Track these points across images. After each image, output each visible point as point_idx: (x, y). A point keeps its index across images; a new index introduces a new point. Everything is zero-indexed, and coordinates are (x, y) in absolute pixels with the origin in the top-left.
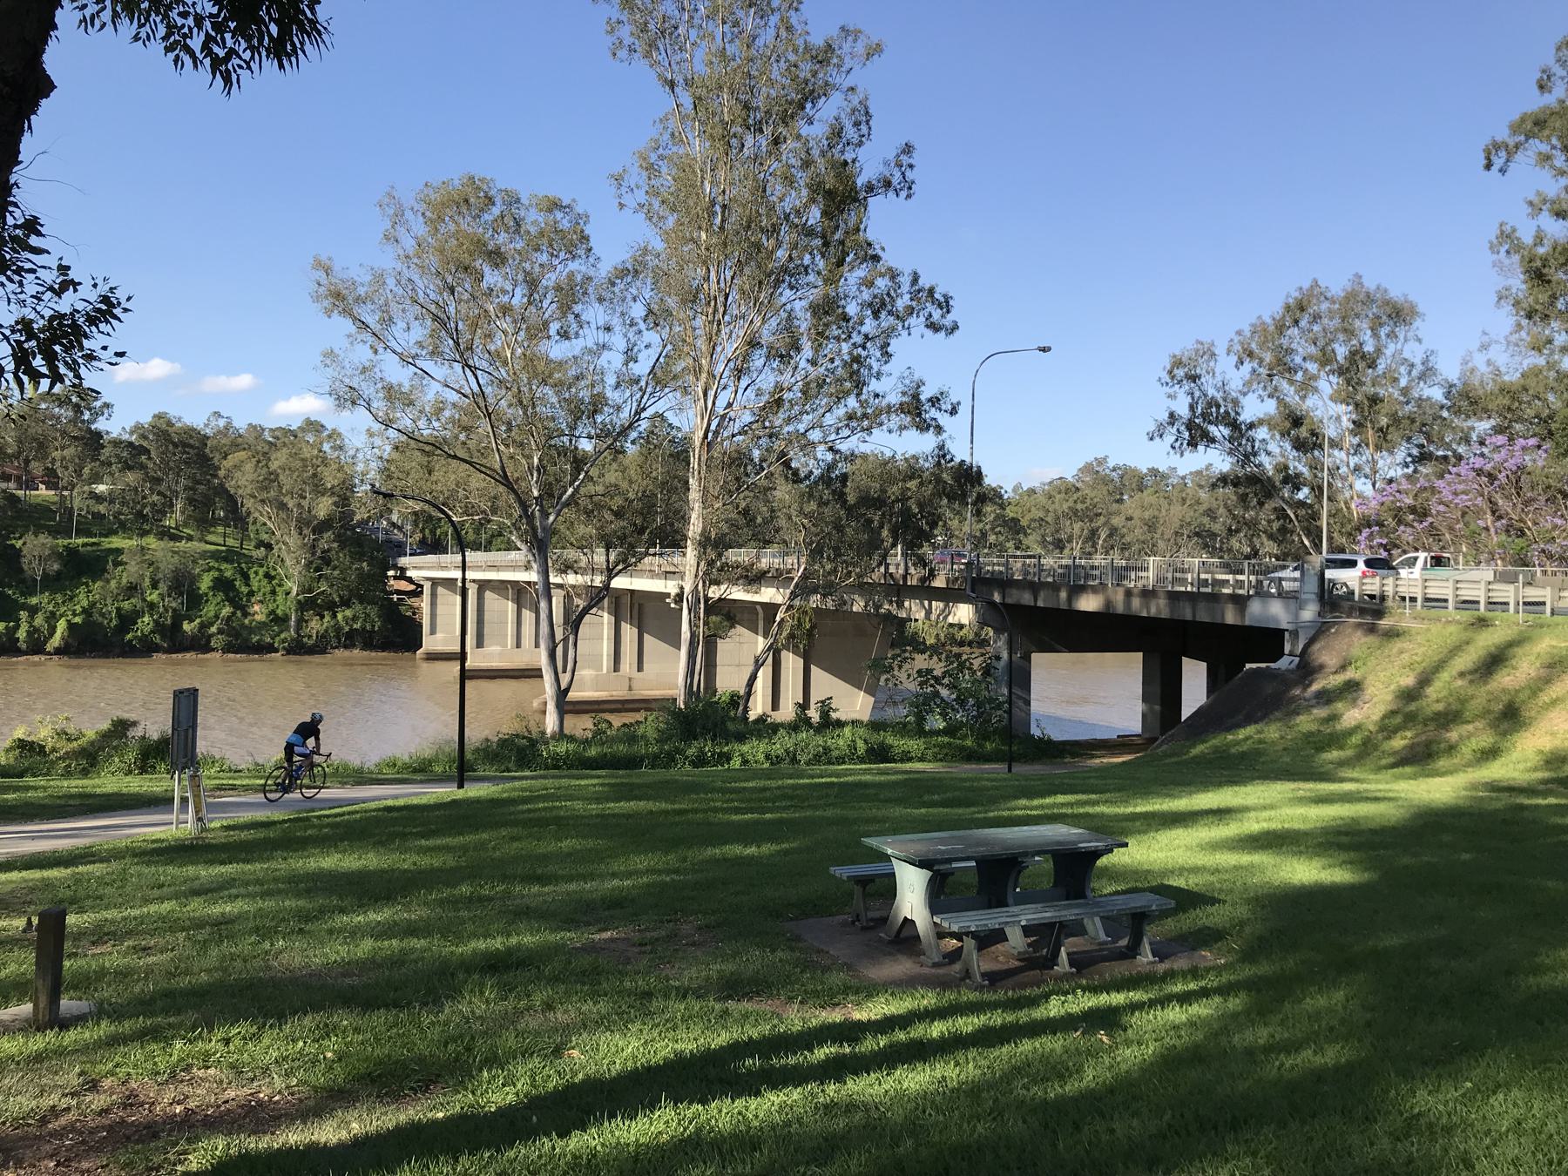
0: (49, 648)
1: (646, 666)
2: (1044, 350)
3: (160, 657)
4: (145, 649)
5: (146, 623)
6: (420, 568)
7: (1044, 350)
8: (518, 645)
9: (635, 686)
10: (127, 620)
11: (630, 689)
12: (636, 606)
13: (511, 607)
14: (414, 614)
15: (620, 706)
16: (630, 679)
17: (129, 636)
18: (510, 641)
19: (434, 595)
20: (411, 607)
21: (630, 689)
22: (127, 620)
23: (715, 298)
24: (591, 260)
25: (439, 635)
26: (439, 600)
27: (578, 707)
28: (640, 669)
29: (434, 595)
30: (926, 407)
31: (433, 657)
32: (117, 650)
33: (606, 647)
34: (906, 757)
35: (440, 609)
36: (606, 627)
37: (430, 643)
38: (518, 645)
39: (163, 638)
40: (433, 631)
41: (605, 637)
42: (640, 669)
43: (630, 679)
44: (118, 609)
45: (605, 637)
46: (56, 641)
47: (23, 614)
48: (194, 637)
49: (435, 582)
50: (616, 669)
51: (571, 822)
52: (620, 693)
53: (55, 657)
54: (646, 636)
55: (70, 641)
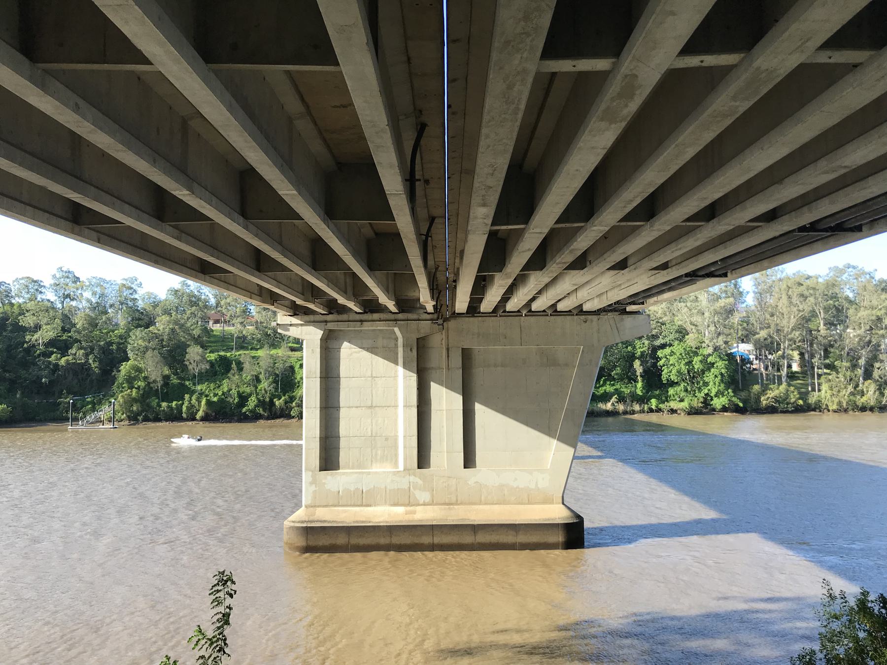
0: (198, 417)
3: (262, 422)
4: (254, 417)
5: (252, 402)
8: (423, 460)
10: (243, 399)
17: (244, 410)
22: (243, 399)
24: (874, 292)
28: (469, 461)
32: (236, 418)
34: (480, 286)
36: (401, 410)
38: (423, 460)
39: (264, 410)
42: (469, 461)
44: (238, 392)
46: (200, 414)
47: (187, 396)
48: (282, 409)
53: (201, 423)
54: (479, 409)
55: (210, 412)
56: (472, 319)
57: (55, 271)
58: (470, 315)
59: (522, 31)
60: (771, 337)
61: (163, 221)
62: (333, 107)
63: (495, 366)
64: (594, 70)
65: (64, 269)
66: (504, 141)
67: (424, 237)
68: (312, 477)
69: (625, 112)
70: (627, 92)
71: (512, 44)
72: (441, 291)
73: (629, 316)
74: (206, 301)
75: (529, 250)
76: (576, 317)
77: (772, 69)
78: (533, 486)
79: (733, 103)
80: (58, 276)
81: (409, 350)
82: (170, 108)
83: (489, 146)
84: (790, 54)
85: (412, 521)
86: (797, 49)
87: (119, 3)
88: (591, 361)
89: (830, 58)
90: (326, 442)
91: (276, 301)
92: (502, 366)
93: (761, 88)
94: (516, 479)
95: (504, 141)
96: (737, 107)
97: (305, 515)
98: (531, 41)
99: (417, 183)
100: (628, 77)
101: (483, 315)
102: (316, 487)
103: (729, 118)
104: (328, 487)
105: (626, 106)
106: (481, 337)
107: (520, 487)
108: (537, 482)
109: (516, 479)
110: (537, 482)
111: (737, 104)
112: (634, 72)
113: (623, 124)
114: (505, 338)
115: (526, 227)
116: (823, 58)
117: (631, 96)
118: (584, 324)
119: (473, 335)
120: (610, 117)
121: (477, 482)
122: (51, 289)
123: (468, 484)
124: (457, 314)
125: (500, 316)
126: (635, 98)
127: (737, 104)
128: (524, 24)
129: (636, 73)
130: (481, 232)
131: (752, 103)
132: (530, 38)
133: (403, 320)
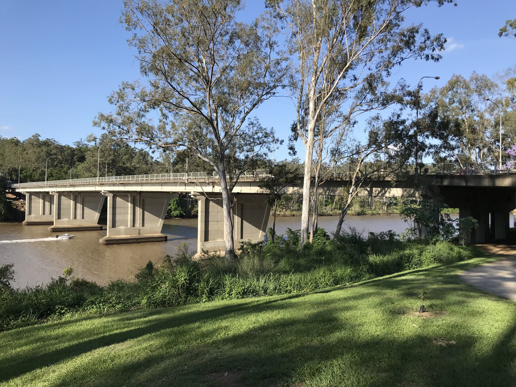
1: (145, 224)
2: (437, 78)
6: (22, 188)
7: (437, 78)
8: (75, 218)
9: (141, 232)
11: (139, 234)
12: (142, 200)
13: (72, 202)
14: (17, 207)
15: (135, 241)
16: (139, 230)
18: (72, 216)
19: (30, 199)
20: (15, 205)
21: (139, 234)
23: (435, 277)
25: (33, 215)
26: (33, 201)
27: (119, 242)
28: (143, 225)
29: (30, 199)
30: (384, 198)
31: (30, 224)
33: (130, 217)
35: (33, 205)
37: (28, 218)
38: (75, 218)
40: (30, 213)
41: (129, 212)
42: (143, 225)
43: (139, 230)
45: (129, 212)
49: (31, 194)
50: (134, 226)
51: (268, 263)
52: (135, 235)
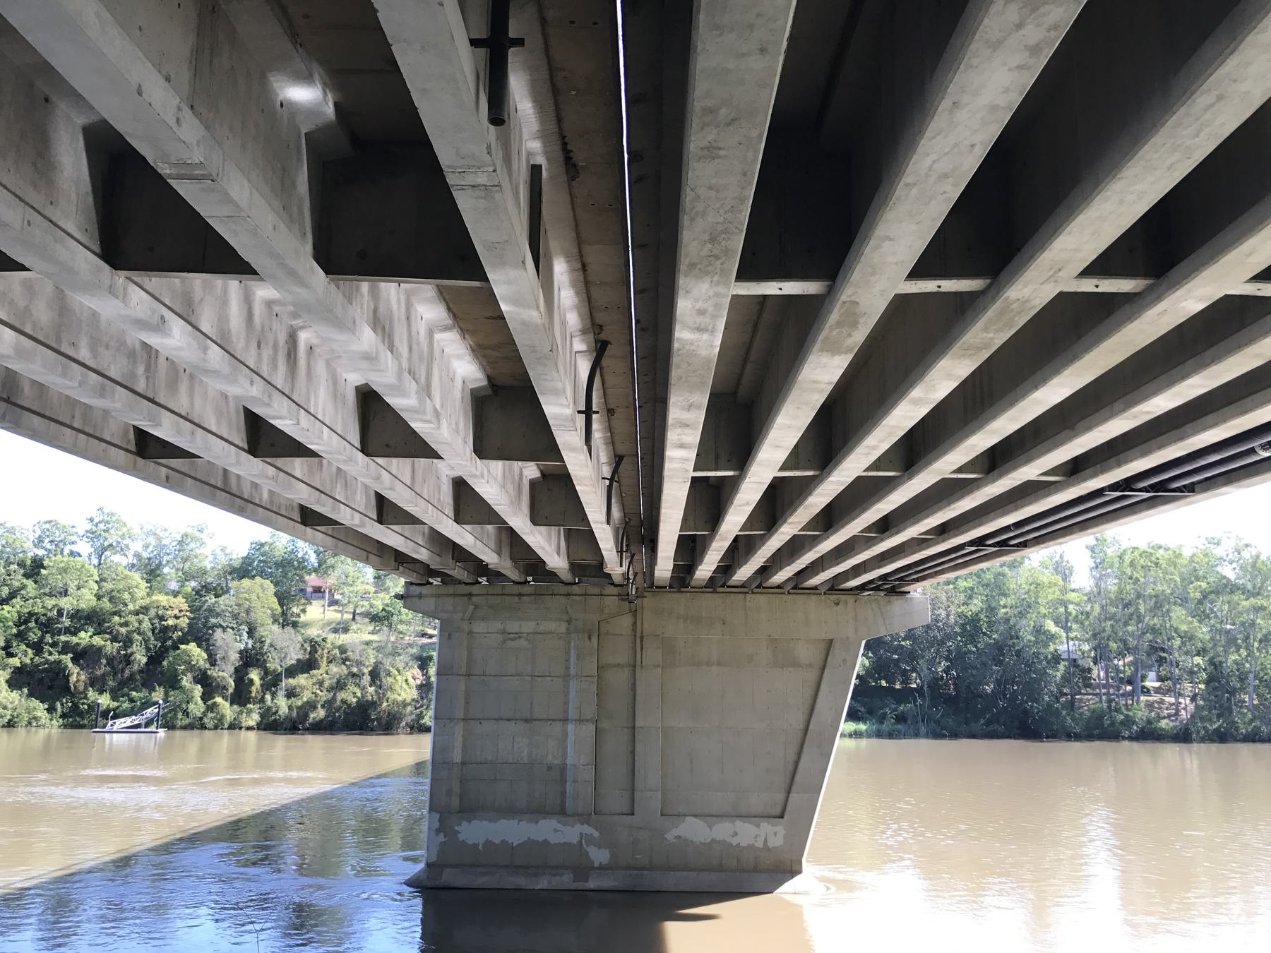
56: (677, 595)
57: (93, 513)
58: (675, 590)
59: (710, 254)
60: (1220, 631)
61: (255, 456)
62: (488, 318)
63: (708, 664)
64: (806, 293)
65: (106, 511)
66: (699, 372)
67: (607, 482)
68: (439, 821)
69: (849, 341)
70: (851, 321)
71: (698, 266)
72: (634, 554)
73: (899, 597)
74: (304, 560)
75: (747, 504)
76: (823, 597)
77: (1024, 299)
78: (760, 844)
79: (985, 335)
80: (96, 520)
81: (586, 639)
82: (192, 106)
83: (681, 378)
84: (1042, 284)
85: (160, 277)
86: (1048, 279)
87: (230, 214)
88: (844, 660)
89: (1097, 286)
90: (462, 770)
91: (403, 563)
92: (719, 664)
93: (1016, 319)
94: (736, 834)
95: (699, 372)
96: (992, 339)
97: (428, 877)
98: (722, 264)
99: (594, 416)
100: (847, 304)
101: (692, 590)
102: (445, 837)
103: (984, 351)
104: (461, 837)
105: (850, 335)
106: (689, 621)
107: (741, 845)
108: (766, 839)
109: (736, 834)
110: (766, 839)
111: (991, 335)
112: (853, 298)
113: (850, 357)
114: (724, 624)
115: (740, 475)
116: (1088, 286)
117: (854, 325)
118: (835, 608)
119: (677, 618)
120: (834, 349)
121: (680, 837)
122: (85, 539)
123: (666, 839)
124: (656, 587)
125: (753, 593)
126: (860, 327)
127: (991, 335)
128: (710, 246)
129: (857, 300)
130: (680, 480)
131: (1009, 336)
132: (720, 261)
133: (579, 595)
